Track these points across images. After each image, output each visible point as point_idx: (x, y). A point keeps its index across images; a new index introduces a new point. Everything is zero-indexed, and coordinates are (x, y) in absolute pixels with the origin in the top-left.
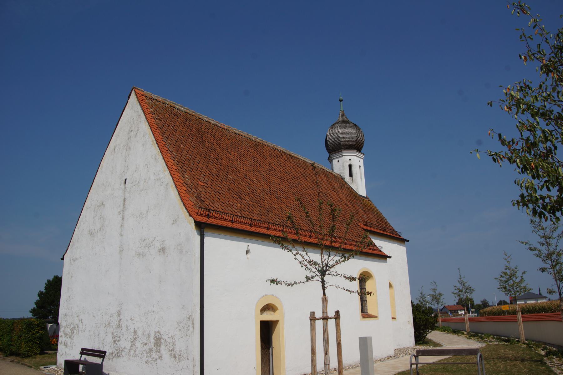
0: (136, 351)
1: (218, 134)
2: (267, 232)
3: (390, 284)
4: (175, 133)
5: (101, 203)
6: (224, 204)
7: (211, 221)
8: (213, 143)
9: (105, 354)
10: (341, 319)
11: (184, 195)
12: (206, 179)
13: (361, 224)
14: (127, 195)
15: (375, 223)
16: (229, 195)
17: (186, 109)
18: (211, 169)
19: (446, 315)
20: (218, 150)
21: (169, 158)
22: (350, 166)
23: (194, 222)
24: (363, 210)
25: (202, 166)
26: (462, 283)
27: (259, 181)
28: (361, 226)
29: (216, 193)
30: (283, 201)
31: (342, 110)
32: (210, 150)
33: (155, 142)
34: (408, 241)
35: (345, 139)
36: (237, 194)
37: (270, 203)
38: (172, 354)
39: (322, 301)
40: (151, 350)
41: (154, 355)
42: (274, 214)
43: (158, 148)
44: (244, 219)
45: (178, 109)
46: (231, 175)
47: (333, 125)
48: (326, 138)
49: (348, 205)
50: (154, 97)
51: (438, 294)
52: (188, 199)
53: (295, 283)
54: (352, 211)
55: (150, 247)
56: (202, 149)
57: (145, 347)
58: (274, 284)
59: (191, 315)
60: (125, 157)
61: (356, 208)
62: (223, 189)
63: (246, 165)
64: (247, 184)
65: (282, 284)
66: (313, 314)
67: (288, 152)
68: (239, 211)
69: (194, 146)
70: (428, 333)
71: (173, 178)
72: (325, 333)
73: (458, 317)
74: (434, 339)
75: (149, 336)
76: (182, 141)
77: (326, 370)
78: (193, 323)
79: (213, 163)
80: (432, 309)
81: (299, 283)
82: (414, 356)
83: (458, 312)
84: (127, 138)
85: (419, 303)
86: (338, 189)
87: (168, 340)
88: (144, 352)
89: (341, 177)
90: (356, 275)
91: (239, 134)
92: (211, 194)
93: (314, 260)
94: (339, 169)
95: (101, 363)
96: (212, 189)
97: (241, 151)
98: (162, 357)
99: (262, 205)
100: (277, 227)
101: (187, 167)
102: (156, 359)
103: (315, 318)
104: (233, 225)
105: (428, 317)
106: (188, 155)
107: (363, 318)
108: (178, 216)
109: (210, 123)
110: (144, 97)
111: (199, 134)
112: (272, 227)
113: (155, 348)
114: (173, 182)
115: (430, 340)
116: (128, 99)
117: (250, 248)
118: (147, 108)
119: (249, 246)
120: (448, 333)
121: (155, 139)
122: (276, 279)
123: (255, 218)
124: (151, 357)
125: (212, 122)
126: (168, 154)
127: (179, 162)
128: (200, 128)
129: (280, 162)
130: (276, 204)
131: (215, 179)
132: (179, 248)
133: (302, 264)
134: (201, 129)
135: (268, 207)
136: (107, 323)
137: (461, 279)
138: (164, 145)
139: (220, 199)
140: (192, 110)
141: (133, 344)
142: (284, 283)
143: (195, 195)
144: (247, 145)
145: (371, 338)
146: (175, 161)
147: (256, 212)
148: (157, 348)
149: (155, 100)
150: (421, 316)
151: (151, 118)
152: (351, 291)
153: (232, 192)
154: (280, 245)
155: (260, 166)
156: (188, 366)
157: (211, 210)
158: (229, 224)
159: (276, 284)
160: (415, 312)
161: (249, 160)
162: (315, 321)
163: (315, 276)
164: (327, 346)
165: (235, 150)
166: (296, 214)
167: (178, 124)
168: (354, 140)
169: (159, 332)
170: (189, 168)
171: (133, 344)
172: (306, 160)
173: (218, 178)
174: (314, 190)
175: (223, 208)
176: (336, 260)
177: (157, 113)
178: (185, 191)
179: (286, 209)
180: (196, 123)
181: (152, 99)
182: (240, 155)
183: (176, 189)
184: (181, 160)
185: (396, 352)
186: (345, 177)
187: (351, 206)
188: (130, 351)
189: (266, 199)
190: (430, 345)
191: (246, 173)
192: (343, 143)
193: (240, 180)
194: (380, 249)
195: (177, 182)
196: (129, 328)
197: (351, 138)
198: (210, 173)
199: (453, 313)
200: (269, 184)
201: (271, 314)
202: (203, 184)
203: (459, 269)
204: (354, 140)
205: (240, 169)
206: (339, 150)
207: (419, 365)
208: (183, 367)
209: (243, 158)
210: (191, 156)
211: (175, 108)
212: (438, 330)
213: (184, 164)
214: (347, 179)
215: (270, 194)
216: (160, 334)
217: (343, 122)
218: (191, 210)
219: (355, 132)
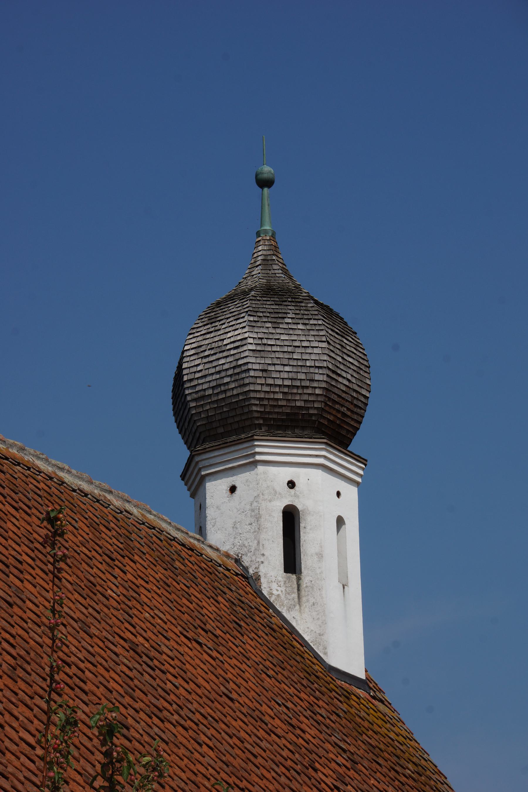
24: (344, 751)
31: (266, 232)
35: (270, 381)
47: (218, 304)
48: (180, 368)
49: (267, 719)
54: (285, 753)
61: (307, 736)
86: (218, 632)
94: (234, 527)
172: (61, 474)
186: (262, 570)
192: (260, 399)
197: (303, 376)
204: (315, 384)
206: (237, 432)
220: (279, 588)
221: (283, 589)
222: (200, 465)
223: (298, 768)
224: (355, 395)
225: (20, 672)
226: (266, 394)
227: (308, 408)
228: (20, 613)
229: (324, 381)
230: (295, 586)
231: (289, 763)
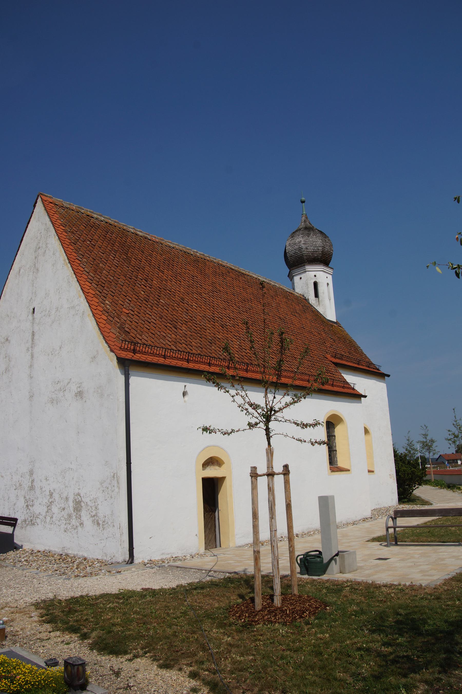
0: (53, 518)
1: (147, 249)
2: (209, 369)
3: (365, 429)
4: (92, 249)
5: (6, 338)
6: (154, 335)
7: (137, 357)
8: (141, 260)
9: (16, 522)
10: (291, 475)
11: (103, 326)
12: (131, 305)
13: (328, 356)
14: (36, 328)
15: (347, 354)
16: (161, 324)
17: (107, 218)
18: (138, 292)
19: (443, 465)
20: (147, 268)
21: (85, 280)
22: (316, 284)
23: (117, 359)
25: (127, 289)
26: (458, 427)
27: (199, 305)
28: (329, 358)
29: (144, 322)
30: (229, 329)
31: (304, 214)
32: (137, 268)
33: (67, 261)
34: (388, 376)
35: (308, 251)
36: (171, 323)
37: (213, 332)
38: (95, 521)
39: (267, 453)
40: (70, 516)
41: (74, 522)
42: (219, 346)
43: (71, 269)
44: (180, 353)
45: (97, 219)
46: (163, 299)
47: (294, 233)
48: (285, 249)
49: (313, 332)
50: (65, 205)
51: (430, 441)
52: (109, 331)
53: (233, 431)
54: (318, 340)
55: (65, 390)
56: (127, 268)
57: (63, 512)
58: (207, 432)
59: (116, 472)
60: (33, 281)
62: (153, 317)
63: (183, 286)
64: (185, 310)
65: (217, 432)
66: (254, 469)
67: (236, 269)
68: (173, 343)
69: (117, 265)
70: (414, 488)
71: (89, 305)
72: (270, 493)
73: (456, 469)
74: (424, 496)
75: (67, 499)
76: (101, 259)
77: (272, 537)
78: (118, 483)
79: (141, 285)
80: (425, 458)
81: (237, 431)
82: (392, 517)
83: (457, 462)
84: (34, 257)
85: (406, 452)
86: (300, 313)
87: (89, 503)
88: (62, 518)
89: (304, 298)
90: (323, 419)
91: (173, 248)
92: (138, 323)
93: (256, 403)
94: (302, 287)
95: (11, 533)
96: (139, 317)
97: (177, 268)
98: (83, 525)
99: (203, 336)
100: (221, 362)
101: (108, 290)
102: (77, 527)
103: (257, 474)
104: (166, 361)
105: (414, 469)
106: (109, 276)
107: (332, 472)
108: (97, 351)
109: (137, 235)
110: (53, 205)
111: (123, 249)
112: (215, 362)
113: (75, 514)
114: (90, 310)
115: (418, 497)
116: (33, 208)
117: (187, 389)
118: (57, 218)
119: (186, 387)
120: (441, 488)
121: (67, 257)
122: (210, 427)
123: (194, 351)
124: (70, 524)
125: (140, 234)
126: (83, 276)
127: (97, 285)
128: (124, 242)
129: (226, 282)
130: (221, 333)
131: (144, 305)
132: (99, 391)
133: (242, 407)
134: (125, 243)
135: (210, 338)
136: (18, 485)
137: (456, 421)
138: (78, 265)
139: (149, 330)
140: (114, 220)
141: (49, 509)
142: (219, 431)
143: (117, 325)
144: (184, 261)
145: (333, 497)
146: (93, 284)
147: (195, 344)
148: (77, 513)
149: (67, 208)
150: (406, 468)
151: (62, 231)
152: (303, 440)
153: (165, 320)
154: (215, 384)
155: (201, 287)
156: (114, 534)
157: (138, 343)
158: (160, 360)
159: (210, 433)
160: (399, 464)
161: (187, 279)
162: (257, 477)
163: (260, 422)
164: (273, 508)
165: (169, 268)
166: (246, 346)
167: (96, 237)
169: (79, 494)
170: (110, 292)
171: (49, 509)
172: (259, 278)
173: (147, 303)
174: (270, 314)
175: (153, 341)
176: (286, 402)
177: (69, 225)
178: (105, 320)
179: (234, 339)
180: (119, 235)
181: (63, 207)
182: (175, 274)
183: (94, 319)
184: (100, 283)
185: (375, 513)
186: (309, 298)
187: (317, 334)
188: (45, 518)
189: (208, 328)
190: (417, 504)
191: (183, 296)
193: (176, 305)
194: (353, 386)
195: (95, 310)
196: (44, 489)
197: (316, 249)
198: (137, 298)
199: (451, 463)
200: (211, 309)
201: (215, 469)
202: (127, 312)
203: (454, 410)
205: (175, 292)
206: (301, 264)
207: (397, 529)
208: (109, 536)
209: (180, 278)
210: (113, 277)
211: (93, 218)
212: (429, 485)
213: (104, 287)
214: (312, 300)
215: (214, 321)
216: (81, 497)
217: (306, 228)
218: (113, 344)
219: (321, 241)
222: (292, 273)
223: (321, 343)
225: (254, 325)
228: (252, 311)
231: (319, 342)
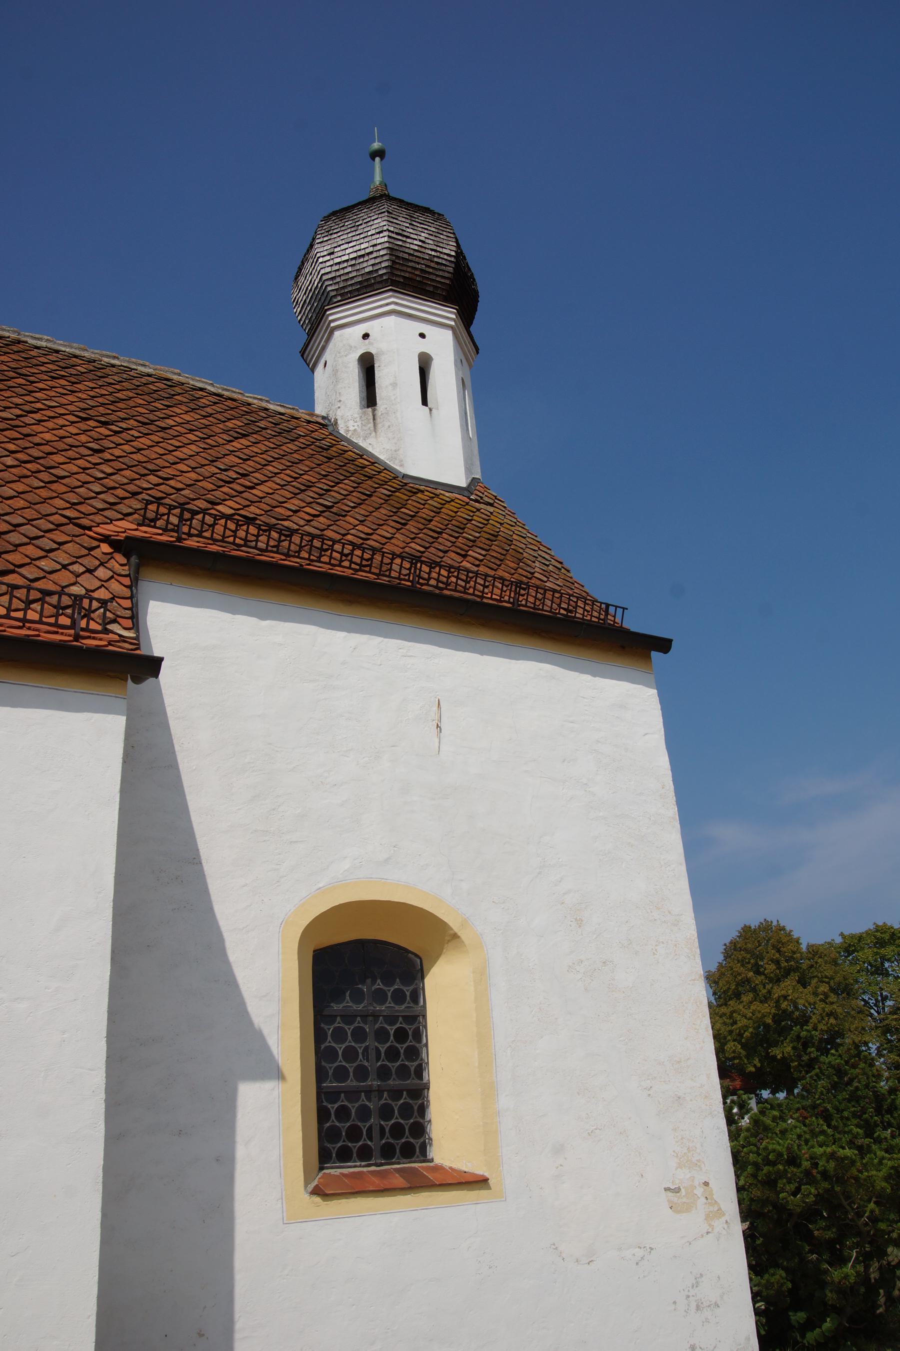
168: (379, 247)
186: (339, 413)
192: (332, 279)
220: (356, 424)
221: (359, 423)
224: (433, 253)
226: (337, 272)
227: (377, 270)
229: (386, 242)
230: (371, 417)
